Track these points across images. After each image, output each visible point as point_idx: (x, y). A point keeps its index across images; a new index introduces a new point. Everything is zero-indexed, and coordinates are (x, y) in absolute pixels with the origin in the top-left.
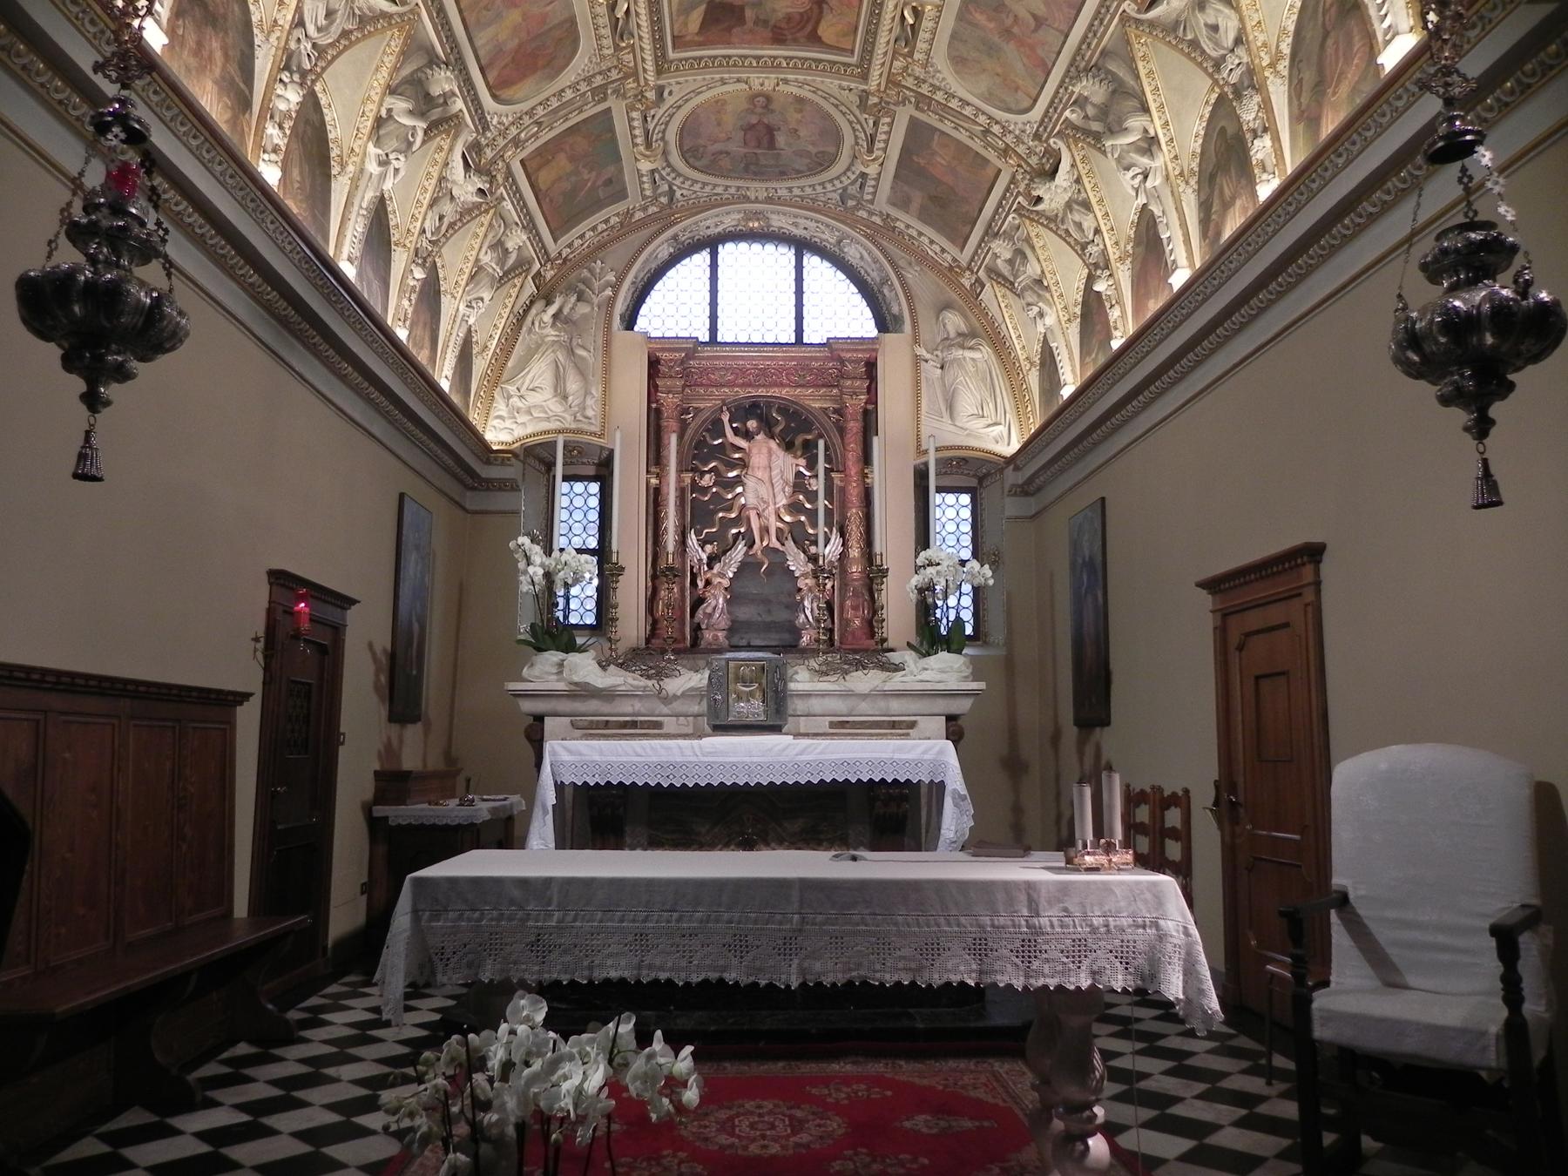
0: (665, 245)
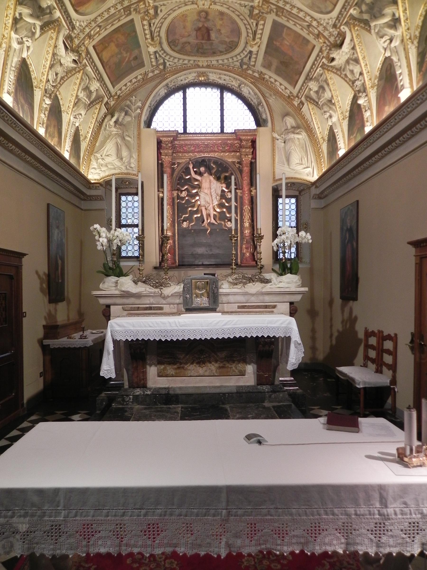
0: (163, 89)
